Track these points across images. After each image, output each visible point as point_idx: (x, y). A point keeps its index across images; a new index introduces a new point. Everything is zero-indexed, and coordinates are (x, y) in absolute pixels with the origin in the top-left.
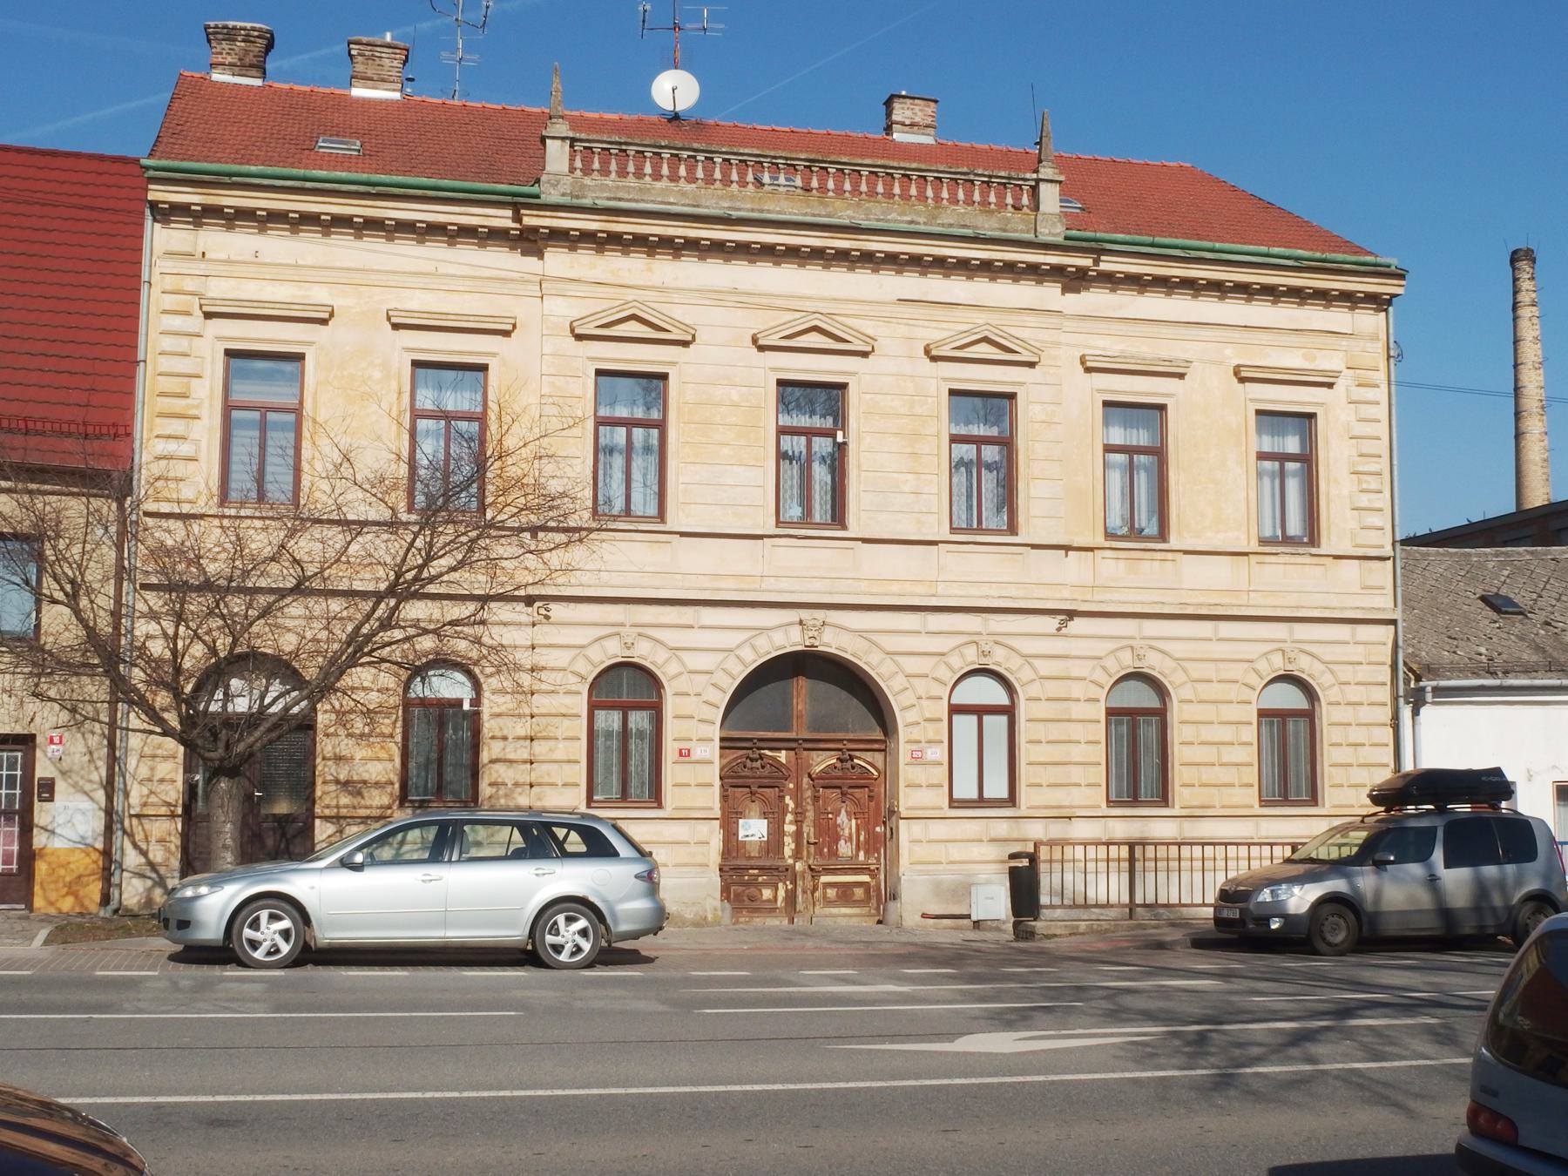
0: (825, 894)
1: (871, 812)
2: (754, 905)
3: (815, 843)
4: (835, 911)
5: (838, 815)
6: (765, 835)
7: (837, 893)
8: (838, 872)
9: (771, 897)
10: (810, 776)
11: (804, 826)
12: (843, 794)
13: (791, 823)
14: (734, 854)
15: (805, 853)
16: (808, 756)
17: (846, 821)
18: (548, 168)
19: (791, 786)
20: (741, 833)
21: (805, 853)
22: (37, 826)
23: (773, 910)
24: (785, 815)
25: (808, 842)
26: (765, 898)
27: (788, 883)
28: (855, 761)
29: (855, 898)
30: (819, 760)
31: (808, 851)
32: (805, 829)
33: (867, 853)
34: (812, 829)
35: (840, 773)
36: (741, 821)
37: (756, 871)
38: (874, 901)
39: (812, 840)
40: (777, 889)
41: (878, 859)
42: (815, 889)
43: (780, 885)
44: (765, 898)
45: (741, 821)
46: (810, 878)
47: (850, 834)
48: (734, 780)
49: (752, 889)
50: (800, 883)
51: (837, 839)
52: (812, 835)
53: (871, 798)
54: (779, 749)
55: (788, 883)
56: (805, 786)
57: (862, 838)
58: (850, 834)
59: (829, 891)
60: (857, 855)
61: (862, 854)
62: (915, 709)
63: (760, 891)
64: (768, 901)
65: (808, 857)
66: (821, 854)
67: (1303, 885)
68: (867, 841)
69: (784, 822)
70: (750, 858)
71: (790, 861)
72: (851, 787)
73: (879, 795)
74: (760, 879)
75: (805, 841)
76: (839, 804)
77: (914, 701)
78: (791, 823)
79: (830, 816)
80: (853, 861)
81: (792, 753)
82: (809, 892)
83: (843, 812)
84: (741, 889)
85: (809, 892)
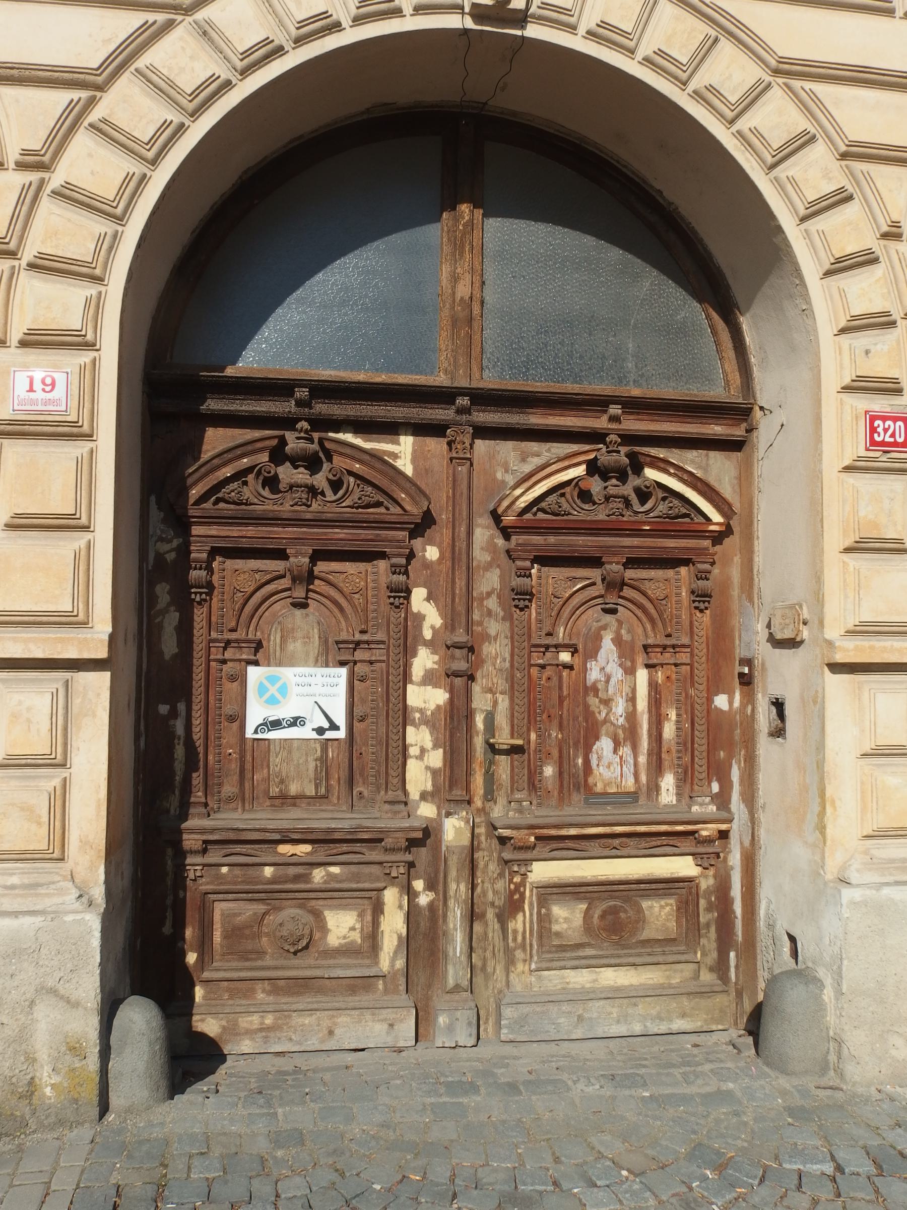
0: (544, 920)
1: (701, 651)
2: (304, 967)
3: (515, 750)
4: (580, 978)
5: (593, 653)
6: (340, 719)
7: (587, 915)
8: (594, 847)
9: (356, 937)
10: (496, 517)
11: (476, 688)
12: (615, 585)
13: (429, 679)
14: (229, 788)
15: (478, 781)
16: (492, 457)
17: (617, 674)
18: (493, 224)
19: (432, 553)
20: (255, 715)
21: (478, 781)
22: (165, 553)
23: (364, 984)
24: (408, 652)
25: (492, 749)
26: (333, 940)
27: (418, 884)
28: (651, 474)
29: (647, 934)
30: (527, 468)
31: (490, 779)
32: (481, 701)
33: (686, 779)
34: (503, 703)
35: (601, 514)
36: (253, 673)
37: (304, 849)
38: (709, 941)
39: (504, 739)
40: (378, 909)
41: (722, 800)
42: (513, 905)
43: (391, 896)
44: (333, 940)
45: (253, 673)
46: (493, 867)
47: (632, 716)
48: (234, 531)
49: (290, 912)
50: (458, 889)
51: (591, 735)
52: (502, 720)
53: (701, 598)
54: (391, 429)
55: (418, 884)
56: (480, 555)
57: (669, 730)
58: (632, 716)
59: (559, 911)
60: (654, 788)
61: (668, 782)
62: (878, 271)
63: (318, 916)
64: (347, 951)
65: (490, 795)
66: (534, 783)
67: (216, 427)
68: (686, 742)
69: (406, 677)
70: (285, 800)
71: (427, 811)
72: (632, 562)
73: (725, 586)
74: (318, 875)
75: (479, 742)
76: (593, 616)
77: (869, 240)
78: (429, 679)
79: (565, 657)
80: (640, 810)
81: (436, 446)
82: (490, 914)
83: (607, 644)
84: (249, 910)
85: (490, 914)
